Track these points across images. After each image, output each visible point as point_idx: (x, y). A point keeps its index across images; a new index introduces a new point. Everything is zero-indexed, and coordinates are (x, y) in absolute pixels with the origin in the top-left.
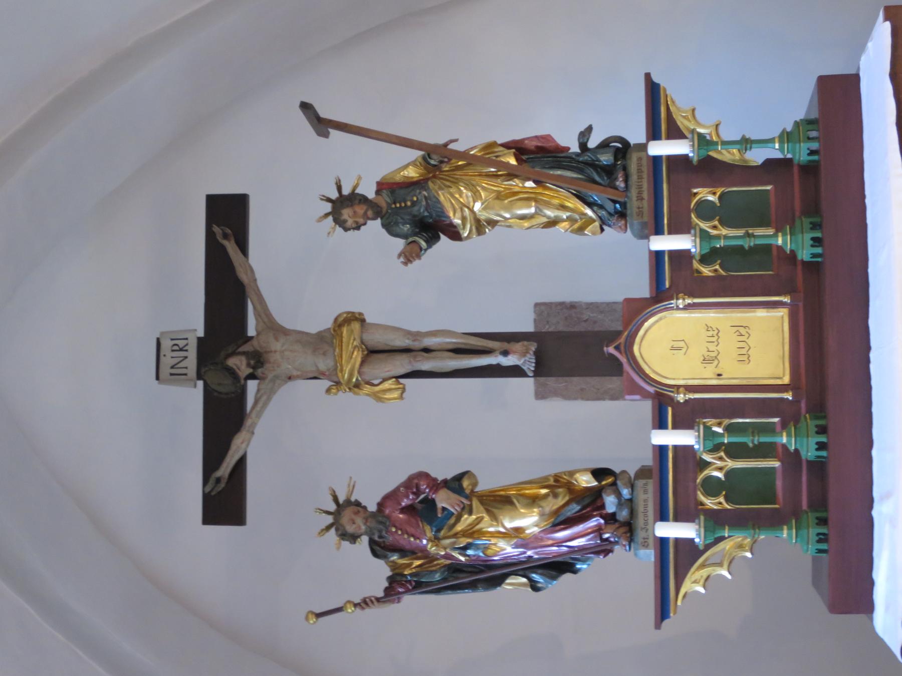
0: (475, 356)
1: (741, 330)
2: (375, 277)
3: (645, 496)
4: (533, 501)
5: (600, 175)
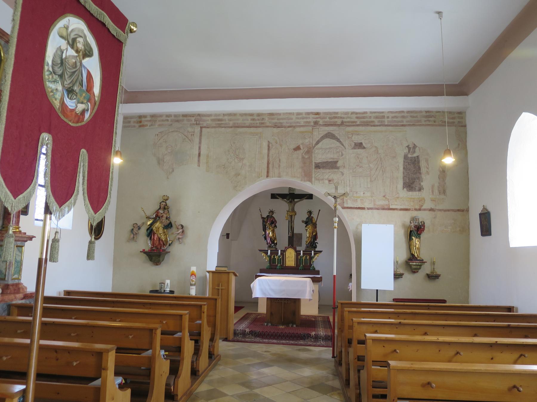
0: (291, 228)
1: (292, 261)
2: (301, 215)
3: (390, 117)
4: (273, 236)
5: (312, 244)
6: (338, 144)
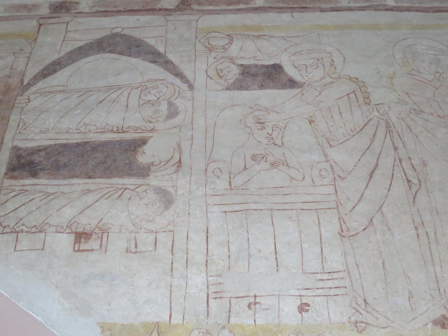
6: (156, 72)
